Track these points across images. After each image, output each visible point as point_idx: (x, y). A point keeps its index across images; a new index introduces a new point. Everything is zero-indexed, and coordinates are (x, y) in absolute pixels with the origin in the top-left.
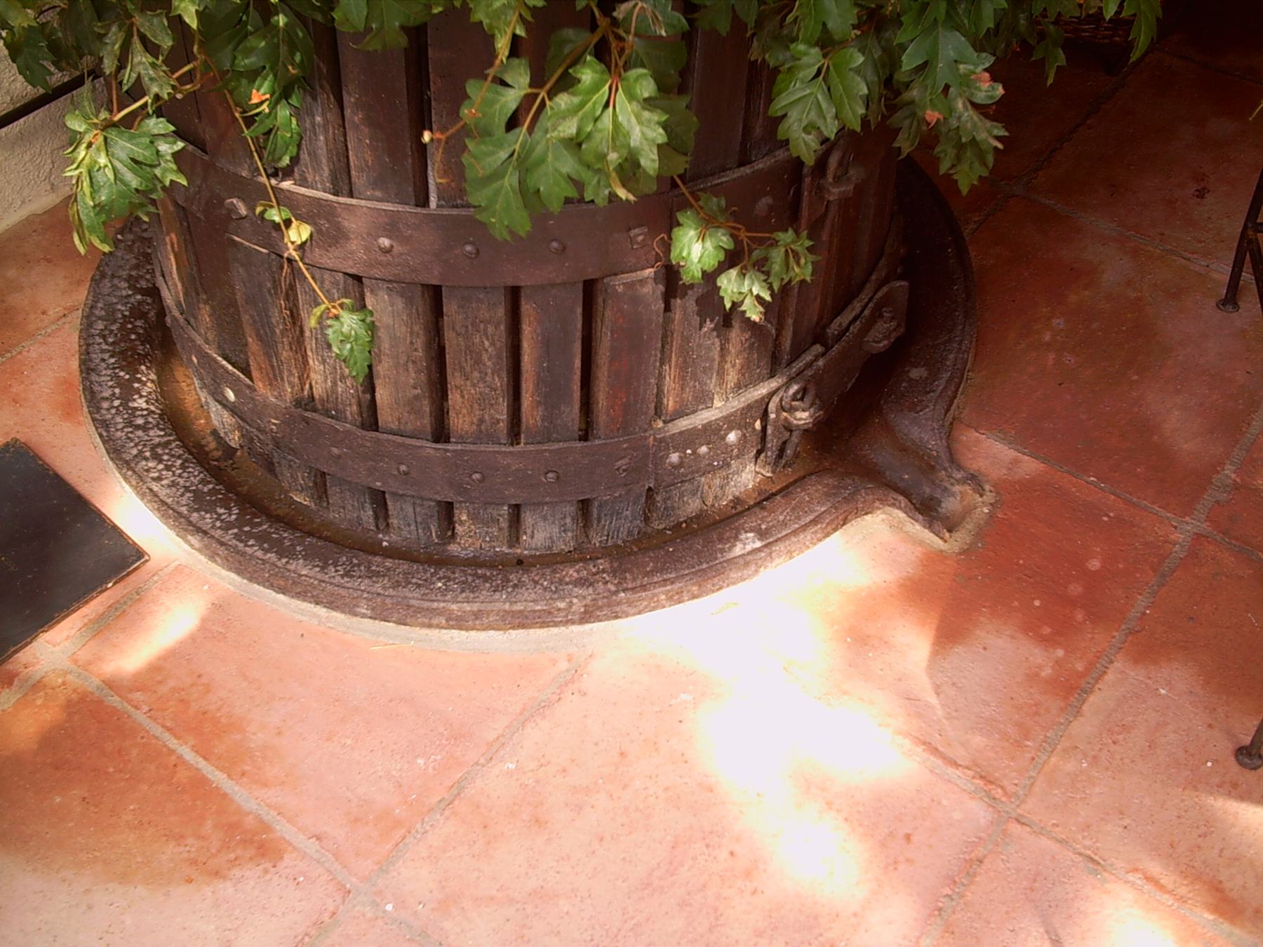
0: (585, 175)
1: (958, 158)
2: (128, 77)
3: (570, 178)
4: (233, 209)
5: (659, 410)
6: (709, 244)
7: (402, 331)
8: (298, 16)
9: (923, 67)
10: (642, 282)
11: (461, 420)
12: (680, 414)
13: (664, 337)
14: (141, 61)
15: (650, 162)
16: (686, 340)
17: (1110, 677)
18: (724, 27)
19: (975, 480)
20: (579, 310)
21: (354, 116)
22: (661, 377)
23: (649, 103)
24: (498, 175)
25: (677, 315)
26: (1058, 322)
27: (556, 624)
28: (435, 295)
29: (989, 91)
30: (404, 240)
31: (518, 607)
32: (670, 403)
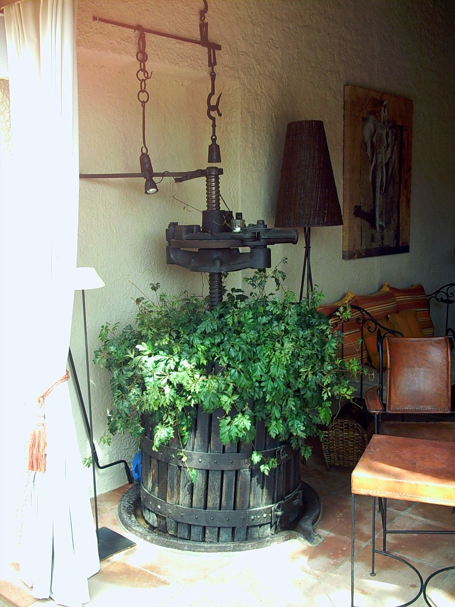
0: (238, 432)
1: (305, 453)
2: (167, 421)
3: (236, 433)
4: (172, 457)
5: (249, 507)
6: (259, 457)
7: (201, 481)
8: (192, 417)
9: (292, 425)
10: (246, 471)
11: (209, 504)
12: (253, 507)
13: (250, 489)
14: (169, 419)
15: (248, 428)
16: (255, 488)
17: (345, 564)
18: (260, 420)
19: (320, 537)
20: (234, 477)
21: (198, 435)
22: (250, 497)
23: (248, 419)
24: (225, 433)
25: (253, 481)
26: (341, 514)
27: (227, 551)
28: (208, 471)
29: (303, 428)
30: (204, 460)
31: (220, 545)
32: (252, 504)
